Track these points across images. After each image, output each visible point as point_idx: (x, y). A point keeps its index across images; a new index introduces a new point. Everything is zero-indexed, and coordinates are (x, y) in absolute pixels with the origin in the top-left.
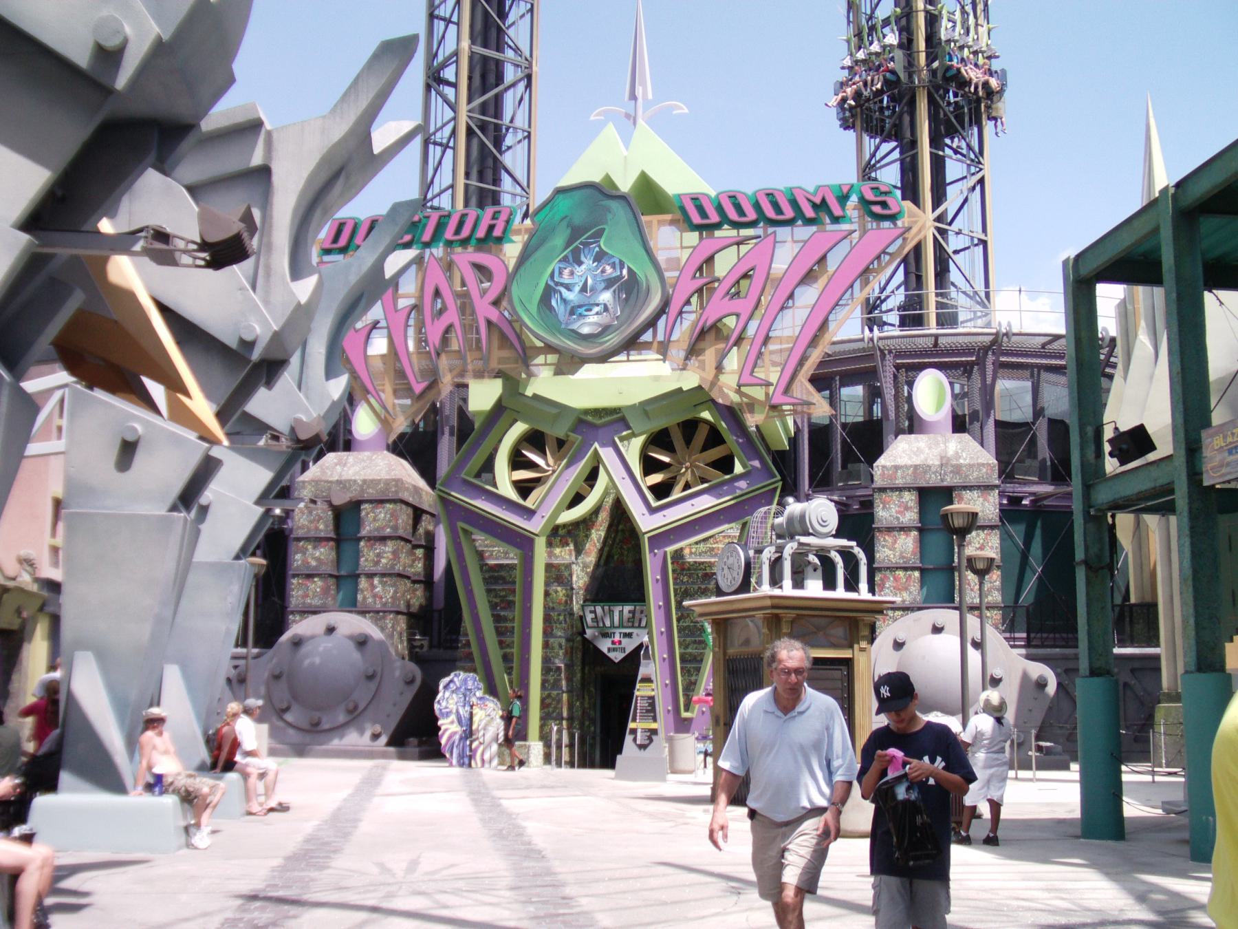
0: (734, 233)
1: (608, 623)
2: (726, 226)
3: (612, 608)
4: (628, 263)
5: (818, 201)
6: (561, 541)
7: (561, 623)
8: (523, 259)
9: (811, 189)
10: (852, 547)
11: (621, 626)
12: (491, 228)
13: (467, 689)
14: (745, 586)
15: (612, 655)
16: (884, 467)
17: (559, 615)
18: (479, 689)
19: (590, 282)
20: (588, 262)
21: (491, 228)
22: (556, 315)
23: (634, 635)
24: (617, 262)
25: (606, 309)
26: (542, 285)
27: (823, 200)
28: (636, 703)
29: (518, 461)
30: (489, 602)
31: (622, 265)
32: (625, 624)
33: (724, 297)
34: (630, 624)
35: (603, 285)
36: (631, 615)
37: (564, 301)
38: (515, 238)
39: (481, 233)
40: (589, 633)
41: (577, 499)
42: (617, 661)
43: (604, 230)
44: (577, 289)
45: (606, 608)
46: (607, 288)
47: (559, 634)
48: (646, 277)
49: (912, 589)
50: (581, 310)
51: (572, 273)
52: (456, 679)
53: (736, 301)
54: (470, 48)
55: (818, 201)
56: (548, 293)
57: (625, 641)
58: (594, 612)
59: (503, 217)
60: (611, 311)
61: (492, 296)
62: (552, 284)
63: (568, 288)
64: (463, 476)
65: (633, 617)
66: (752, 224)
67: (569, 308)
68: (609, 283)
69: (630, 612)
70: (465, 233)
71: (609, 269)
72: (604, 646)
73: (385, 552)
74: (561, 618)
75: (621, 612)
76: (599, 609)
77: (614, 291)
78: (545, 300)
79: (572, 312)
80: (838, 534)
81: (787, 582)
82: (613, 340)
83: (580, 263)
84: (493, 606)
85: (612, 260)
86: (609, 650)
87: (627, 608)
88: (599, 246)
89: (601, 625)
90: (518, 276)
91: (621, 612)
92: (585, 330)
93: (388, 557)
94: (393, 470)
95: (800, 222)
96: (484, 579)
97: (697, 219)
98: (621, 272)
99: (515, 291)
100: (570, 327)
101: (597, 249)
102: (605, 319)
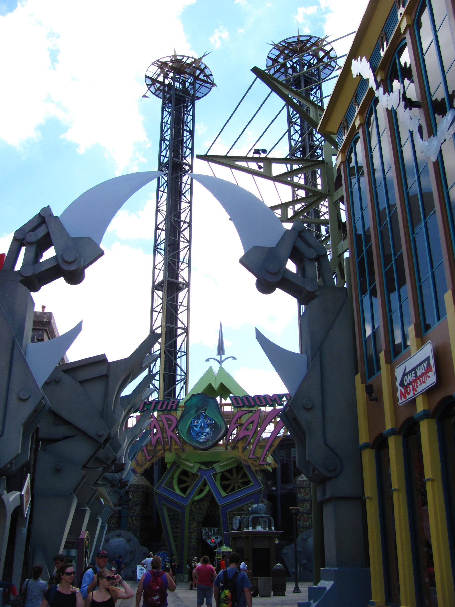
0: (247, 409)
1: (210, 534)
2: (245, 407)
3: (211, 529)
4: (215, 419)
5: (273, 399)
6: (195, 506)
7: (194, 534)
8: (182, 417)
9: (271, 395)
10: (269, 517)
11: (214, 534)
12: (172, 406)
13: (163, 556)
14: (240, 528)
15: (211, 544)
16: (299, 480)
17: (194, 531)
18: (168, 556)
19: (203, 425)
20: (202, 419)
21: (172, 406)
22: (192, 435)
23: (218, 538)
24: (211, 419)
25: (208, 434)
26: (188, 425)
27: (275, 399)
28: (216, 561)
29: (180, 482)
30: (171, 526)
31: (213, 420)
32: (216, 534)
33: (244, 430)
34: (217, 534)
35: (207, 426)
36: (217, 531)
37: (195, 431)
38: (179, 409)
39: (169, 408)
40: (204, 537)
41: (201, 491)
42: (213, 546)
43: (207, 408)
44: (199, 427)
45: (209, 529)
46: (208, 427)
47: (194, 537)
48: (220, 424)
49: (309, 521)
50: (200, 434)
51: (197, 422)
52: (160, 553)
53: (248, 432)
54: (166, 325)
55: (273, 399)
56: (190, 428)
57: (215, 540)
58: (205, 530)
59: (176, 403)
60: (209, 434)
61: (172, 428)
62: (191, 425)
63: (196, 427)
64: (163, 486)
65: (218, 531)
66: (253, 406)
67: (196, 433)
68: (209, 426)
69: (217, 530)
70: (164, 408)
71: (209, 421)
72: (209, 541)
73: (137, 509)
74: (195, 532)
75: (214, 530)
76: (207, 529)
77: (210, 428)
78: (189, 430)
79: (197, 435)
80: (266, 513)
81: (250, 528)
82: (209, 444)
83: (200, 419)
84: (172, 528)
85: (210, 418)
86: (210, 542)
87: (216, 529)
88: (206, 414)
89: (208, 534)
90: (180, 423)
91: (214, 530)
92: (201, 440)
93: (137, 511)
94: (140, 481)
95: (268, 406)
96: (169, 519)
97: (236, 405)
98: (213, 422)
99: (180, 427)
100: (197, 440)
101: (205, 414)
102: (207, 437)
